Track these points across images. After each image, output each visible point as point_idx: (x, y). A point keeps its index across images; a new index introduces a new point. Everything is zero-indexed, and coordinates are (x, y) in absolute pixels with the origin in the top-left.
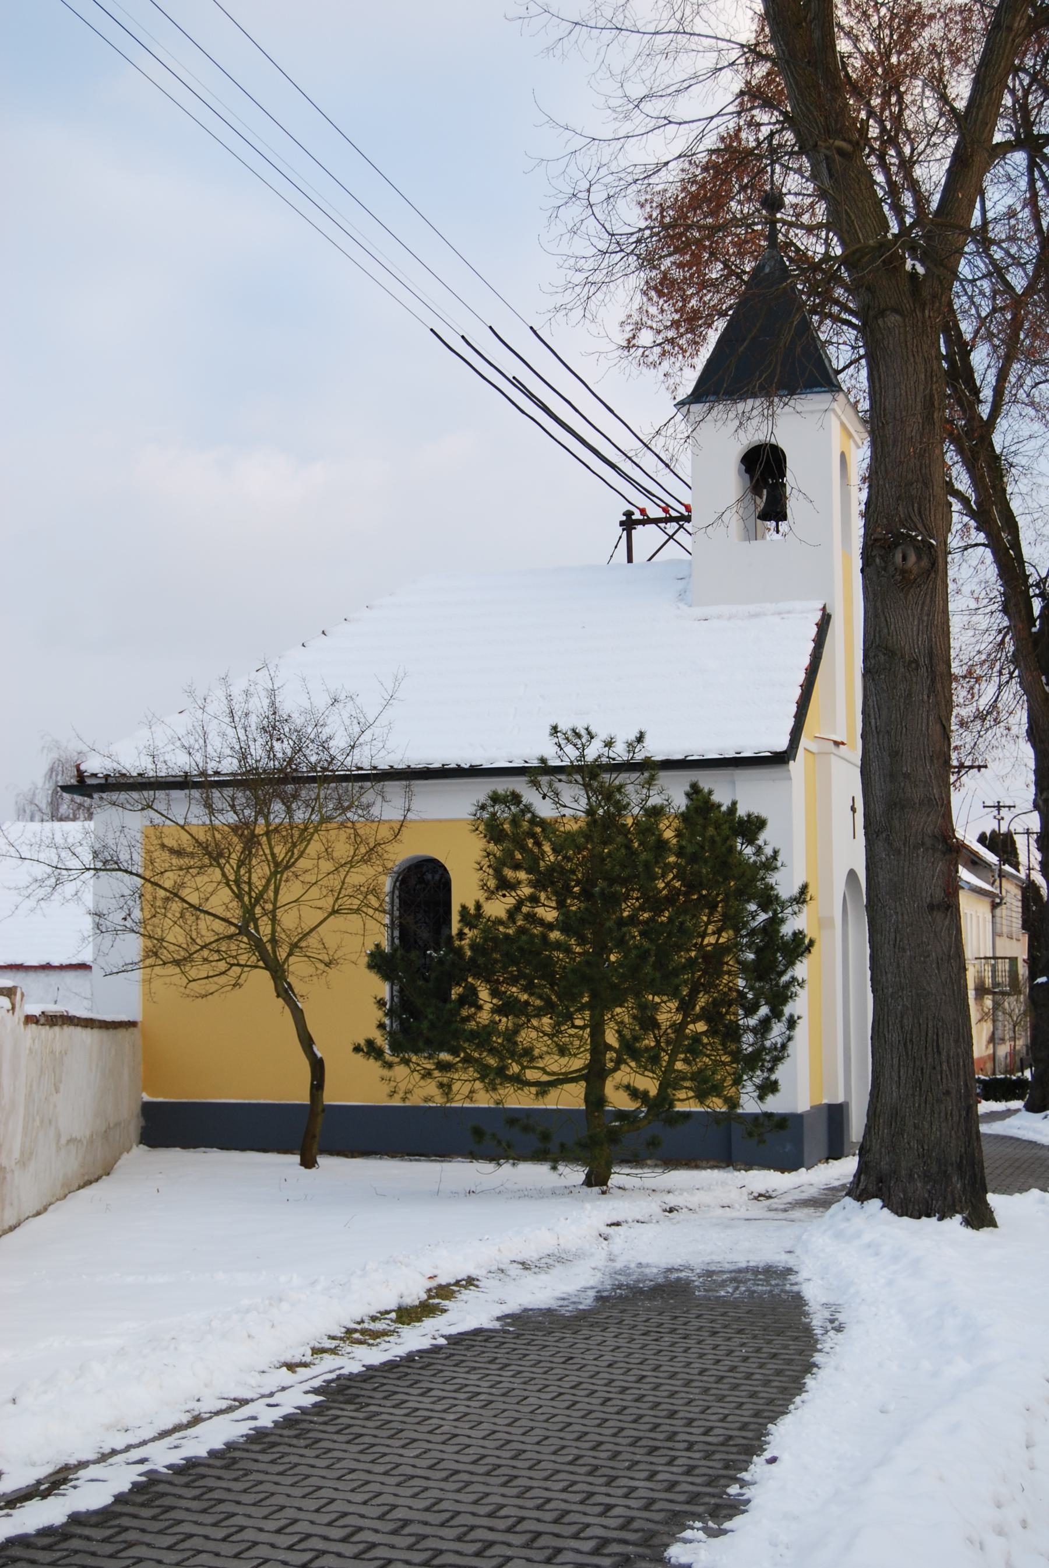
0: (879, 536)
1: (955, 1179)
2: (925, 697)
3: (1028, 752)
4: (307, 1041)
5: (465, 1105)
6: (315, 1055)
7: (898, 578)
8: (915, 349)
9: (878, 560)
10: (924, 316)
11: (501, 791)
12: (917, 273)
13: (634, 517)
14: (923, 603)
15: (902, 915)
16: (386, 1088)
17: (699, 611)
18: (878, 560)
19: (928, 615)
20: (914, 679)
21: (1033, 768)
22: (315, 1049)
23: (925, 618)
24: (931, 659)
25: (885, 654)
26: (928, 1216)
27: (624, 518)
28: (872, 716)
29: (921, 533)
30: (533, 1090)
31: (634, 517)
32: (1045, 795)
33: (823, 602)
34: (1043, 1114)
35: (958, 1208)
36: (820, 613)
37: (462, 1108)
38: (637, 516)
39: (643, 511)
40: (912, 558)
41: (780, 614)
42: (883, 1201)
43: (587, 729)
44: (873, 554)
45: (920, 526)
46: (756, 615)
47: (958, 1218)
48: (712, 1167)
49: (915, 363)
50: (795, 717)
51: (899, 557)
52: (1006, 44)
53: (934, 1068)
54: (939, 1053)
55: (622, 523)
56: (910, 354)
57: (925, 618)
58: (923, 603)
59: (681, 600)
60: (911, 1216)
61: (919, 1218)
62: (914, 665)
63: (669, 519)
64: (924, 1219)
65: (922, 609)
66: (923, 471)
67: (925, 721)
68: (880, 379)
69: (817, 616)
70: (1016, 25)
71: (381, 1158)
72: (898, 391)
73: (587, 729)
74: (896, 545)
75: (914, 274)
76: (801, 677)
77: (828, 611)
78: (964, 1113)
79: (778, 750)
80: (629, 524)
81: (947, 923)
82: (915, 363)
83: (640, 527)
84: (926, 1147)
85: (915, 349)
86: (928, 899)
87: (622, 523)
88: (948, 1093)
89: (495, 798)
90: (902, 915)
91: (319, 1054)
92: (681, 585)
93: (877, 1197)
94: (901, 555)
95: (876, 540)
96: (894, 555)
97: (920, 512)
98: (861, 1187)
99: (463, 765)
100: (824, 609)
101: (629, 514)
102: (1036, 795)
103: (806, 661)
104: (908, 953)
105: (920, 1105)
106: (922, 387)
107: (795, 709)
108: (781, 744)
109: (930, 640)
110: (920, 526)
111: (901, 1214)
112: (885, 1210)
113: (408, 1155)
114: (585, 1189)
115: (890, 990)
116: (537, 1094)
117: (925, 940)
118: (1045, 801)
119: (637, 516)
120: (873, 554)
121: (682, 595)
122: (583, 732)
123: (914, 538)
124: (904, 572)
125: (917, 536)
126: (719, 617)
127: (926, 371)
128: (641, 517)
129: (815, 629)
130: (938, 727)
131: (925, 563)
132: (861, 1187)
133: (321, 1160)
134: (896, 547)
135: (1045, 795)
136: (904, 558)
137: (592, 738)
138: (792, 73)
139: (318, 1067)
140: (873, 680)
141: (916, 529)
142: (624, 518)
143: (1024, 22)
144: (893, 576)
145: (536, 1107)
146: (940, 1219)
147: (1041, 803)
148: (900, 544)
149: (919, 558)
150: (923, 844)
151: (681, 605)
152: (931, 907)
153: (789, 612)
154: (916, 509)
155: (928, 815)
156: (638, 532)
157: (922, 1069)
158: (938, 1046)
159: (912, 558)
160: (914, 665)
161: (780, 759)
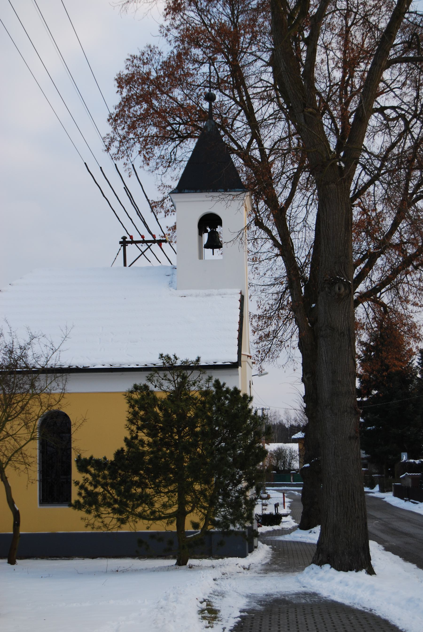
0: (327, 279)
1: (362, 554)
2: (347, 348)
3: (298, 355)
4: (11, 502)
5: (118, 531)
6: (15, 509)
7: (336, 297)
8: (342, 199)
9: (327, 289)
10: (345, 185)
11: (138, 384)
12: (341, 166)
13: (126, 240)
14: (346, 308)
15: (338, 441)
16: (84, 523)
17: (181, 292)
18: (327, 289)
19: (348, 313)
20: (343, 340)
21: (301, 362)
22: (16, 506)
23: (347, 314)
24: (349, 332)
25: (330, 329)
26: (351, 570)
27: (122, 240)
28: (324, 355)
29: (345, 278)
30: (166, 521)
31: (126, 240)
32: (308, 376)
33: (240, 290)
34: (309, 531)
35: (364, 566)
36: (240, 295)
37: (117, 533)
38: (128, 239)
39: (131, 237)
40: (343, 289)
41: (220, 295)
42: (331, 565)
43: (174, 356)
44: (325, 286)
45: (344, 275)
46: (209, 295)
47: (364, 571)
48: (206, 558)
49: (342, 205)
50: (238, 345)
51: (337, 288)
52: (379, 72)
53: (352, 507)
54: (354, 500)
55: (121, 243)
56: (340, 201)
57: (347, 314)
58: (346, 308)
59: (171, 286)
60: (344, 571)
61: (347, 571)
62: (342, 334)
63: (144, 242)
64: (349, 572)
65: (345, 310)
66: (345, 251)
67: (347, 358)
68: (326, 211)
69: (239, 297)
70: (383, 64)
71: (36, 559)
72: (334, 217)
73: (174, 356)
74: (336, 283)
75: (340, 167)
76: (237, 326)
77: (242, 294)
78: (364, 526)
79: (234, 362)
80: (124, 243)
81: (356, 444)
82: (342, 205)
83: (129, 245)
84: (349, 541)
85: (342, 199)
86: (349, 434)
87: (121, 243)
88: (358, 517)
89: (136, 387)
90: (338, 441)
91: (17, 509)
92: (169, 278)
93: (327, 563)
94: (338, 288)
95: (325, 280)
96: (335, 287)
97: (344, 269)
98: (320, 559)
99: (79, 367)
100: (241, 293)
101: (124, 238)
102: (303, 375)
103: (238, 319)
104: (340, 458)
105: (346, 523)
106: (344, 216)
107: (237, 342)
108: (235, 359)
109: (348, 324)
110: (344, 275)
111: (339, 570)
112: (332, 569)
113: (50, 557)
114: (178, 567)
115: (332, 474)
116: (167, 524)
117: (347, 452)
118: (308, 378)
119: (128, 239)
120: (325, 286)
121: (171, 284)
122: (172, 357)
123: (343, 280)
124: (339, 295)
125: (344, 279)
126: (191, 295)
127: (346, 209)
128: (130, 240)
129: (239, 303)
130: (352, 361)
131: (347, 291)
132: (320, 559)
133: (18, 561)
134: (336, 284)
135: (308, 376)
136: (339, 289)
137: (177, 359)
138: (289, 76)
139: (16, 515)
140: (324, 340)
141: (343, 277)
142: (122, 240)
143: (386, 63)
144: (334, 296)
145: (93, 532)
146: (357, 571)
147: (306, 379)
148: (337, 283)
149: (345, 289)
150: (346, 411)
151: (171, 289)
152: (350, 438)
153: (225, 294)
154: (343, 268)
155: (348, 398)
156: (130, 248)
157: (347, 507)
158: (354, 498)
159: (343, 289)
160: (342, 334)
161: (235, 366)
